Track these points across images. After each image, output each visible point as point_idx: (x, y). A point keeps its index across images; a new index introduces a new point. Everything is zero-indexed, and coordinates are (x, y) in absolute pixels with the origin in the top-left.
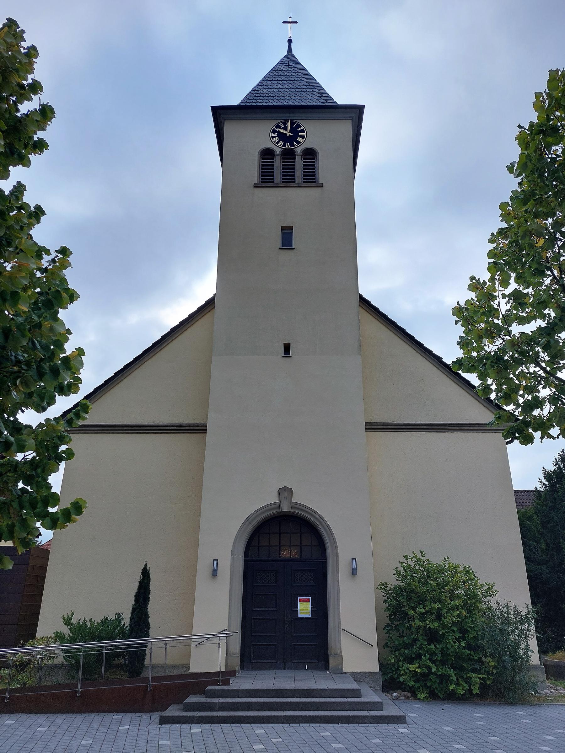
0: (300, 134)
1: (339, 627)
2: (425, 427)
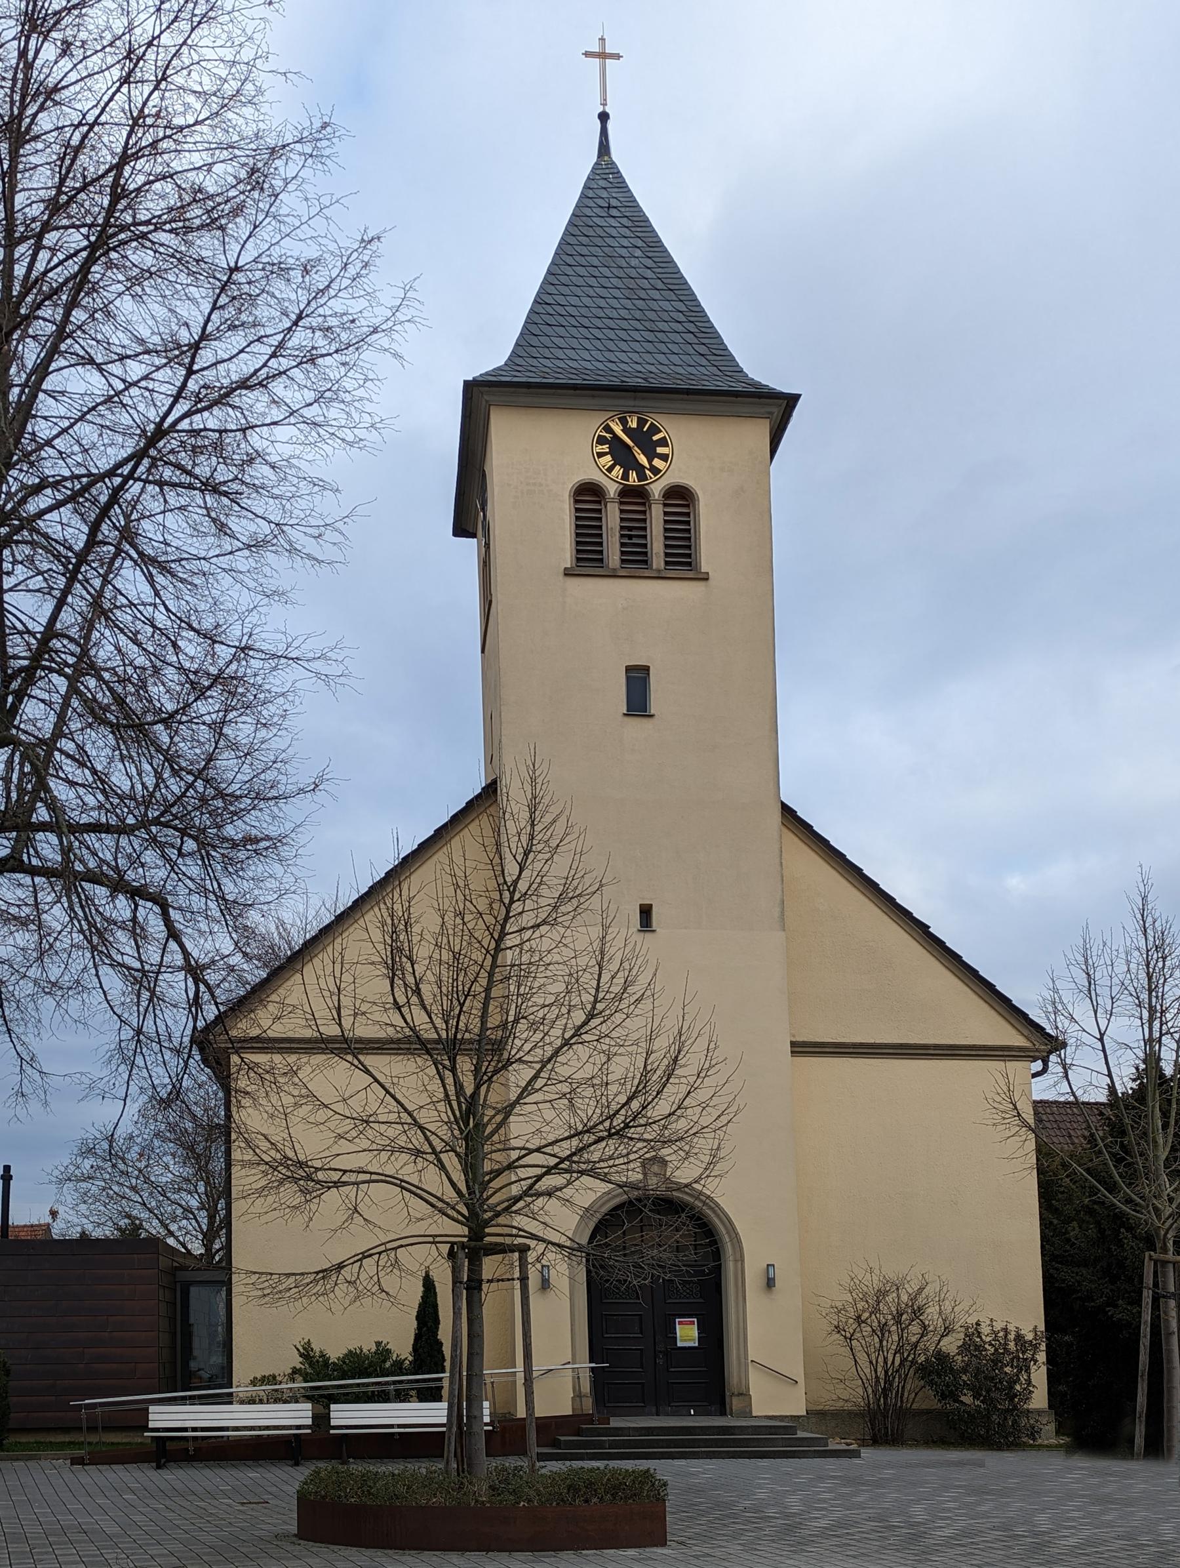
0: (660, 450)
1: (746, 1358)
2: (891, 1051)
